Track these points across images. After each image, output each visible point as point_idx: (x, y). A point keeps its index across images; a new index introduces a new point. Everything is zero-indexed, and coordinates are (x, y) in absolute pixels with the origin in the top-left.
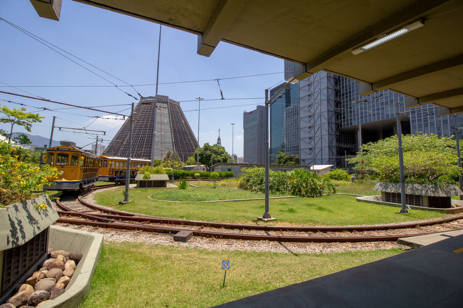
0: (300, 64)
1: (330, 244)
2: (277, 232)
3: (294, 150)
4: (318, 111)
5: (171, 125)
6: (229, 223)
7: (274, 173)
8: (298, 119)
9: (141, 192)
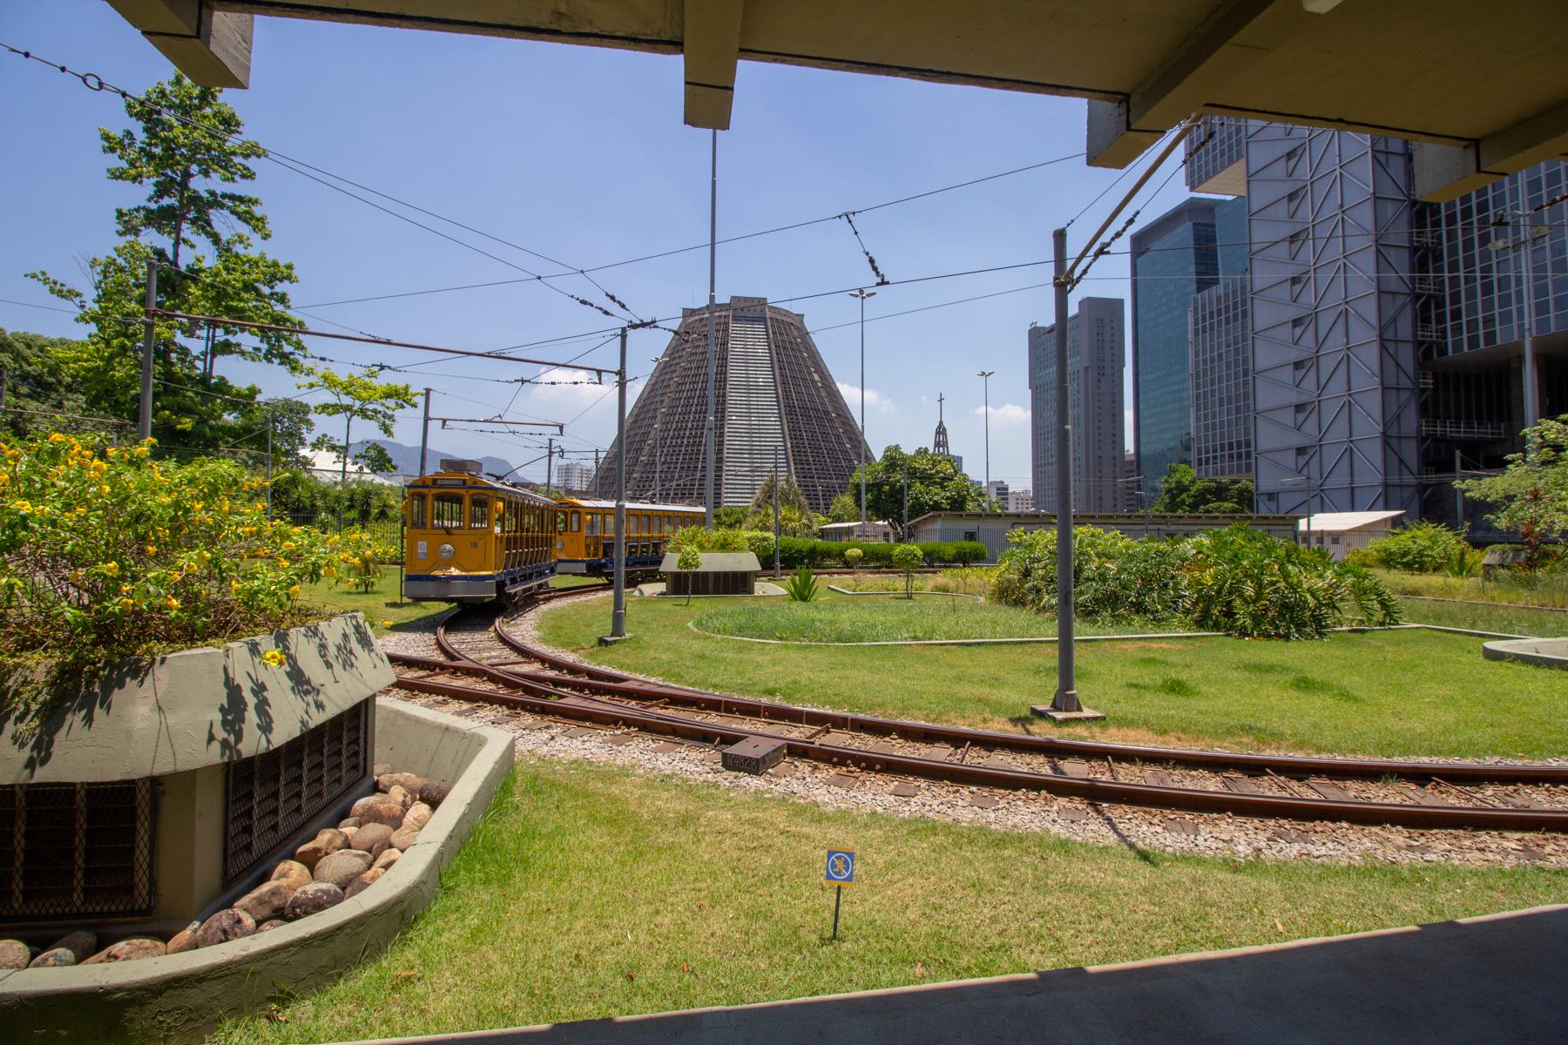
0: (1100, 99)
1: (1309, 825)
2: (1093, 763)
3: (1231, 456)
4: (1336, 296)
5: (780, 391)
6: (923, 723)
7: (1127, 548)
8: (1244, 339)
9: (672, 607)
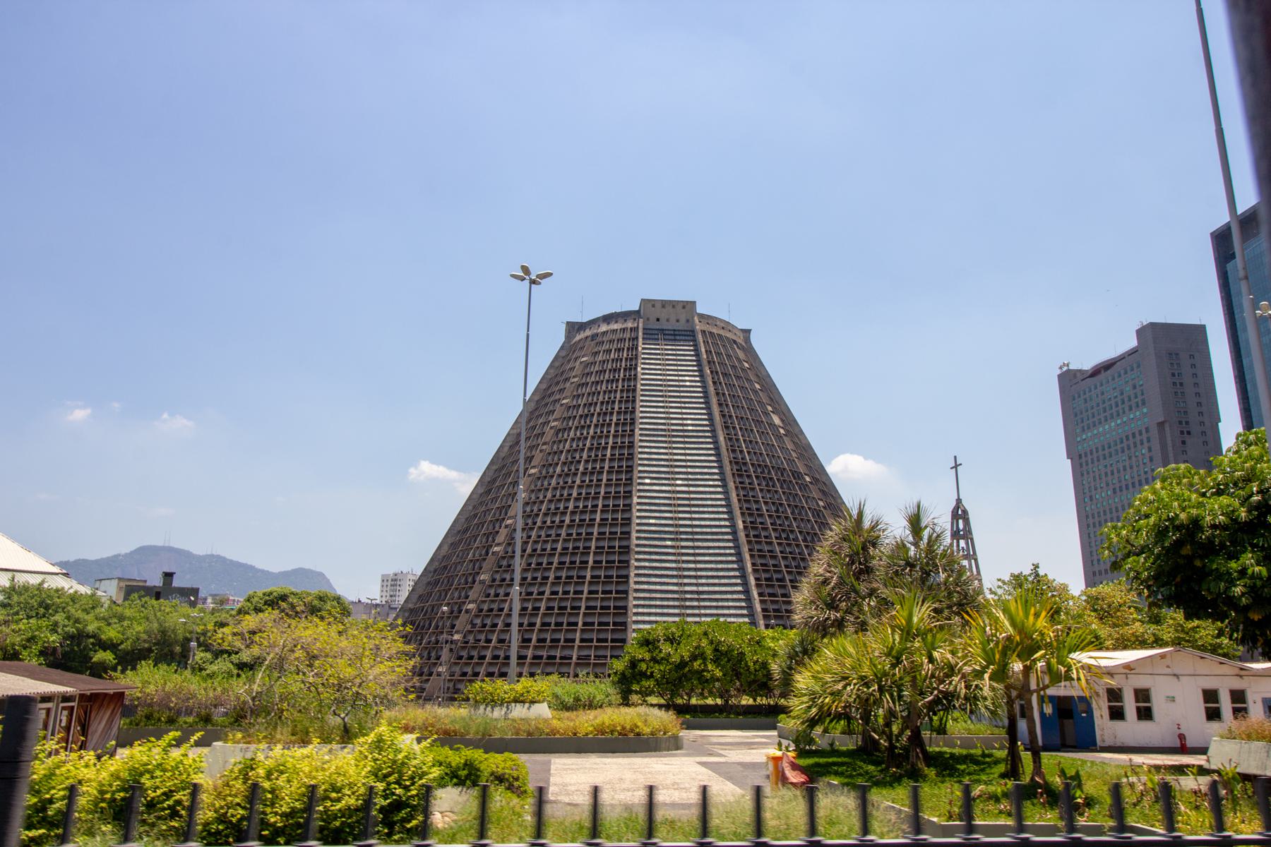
5: (721, 439)
